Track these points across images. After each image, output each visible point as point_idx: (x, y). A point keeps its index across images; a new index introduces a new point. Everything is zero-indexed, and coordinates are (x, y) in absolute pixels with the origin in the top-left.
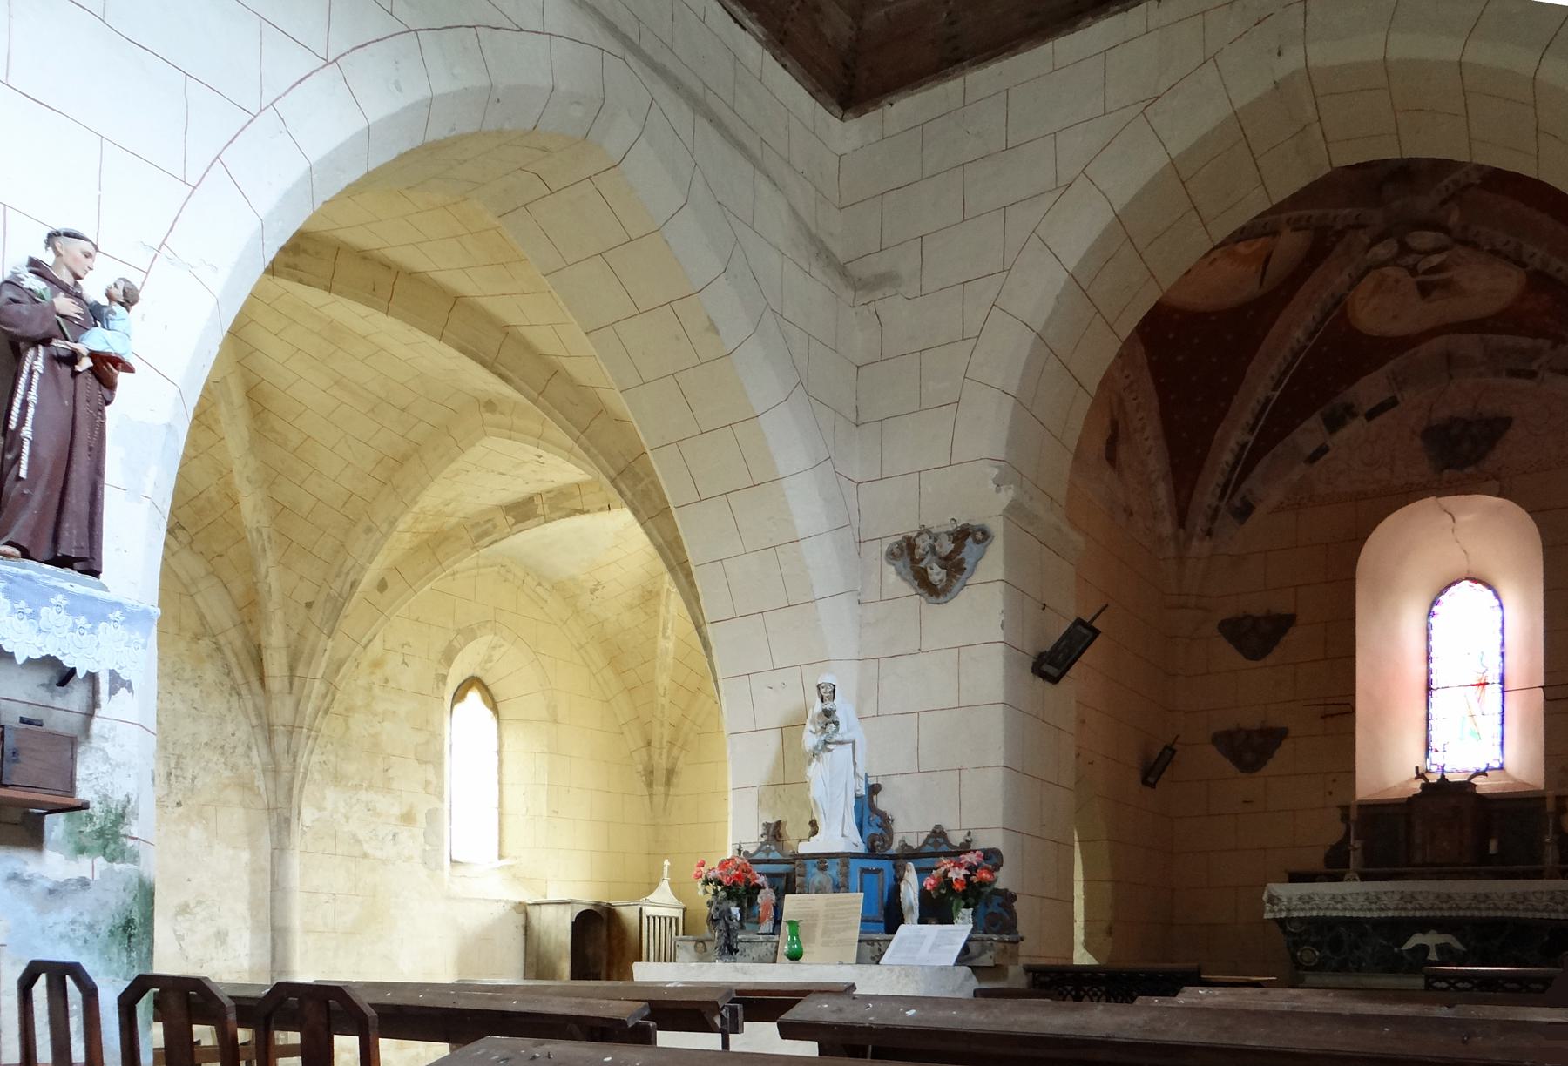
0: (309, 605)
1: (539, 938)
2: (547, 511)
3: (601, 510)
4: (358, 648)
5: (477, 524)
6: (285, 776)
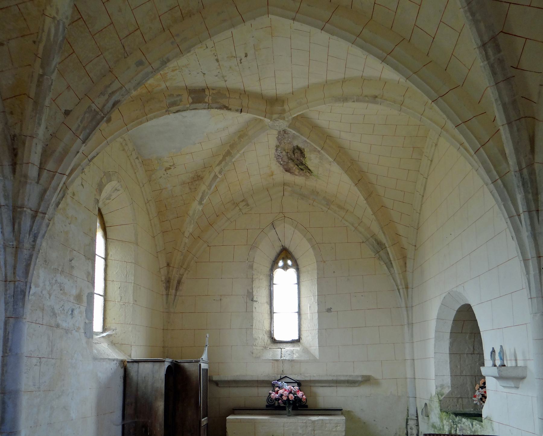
0: (67, 113)
1: (137, 384)
2: (210, 102)
3: (237, 111)
4: (86, 161)
5: (171, 95)
6: (26, 253)
